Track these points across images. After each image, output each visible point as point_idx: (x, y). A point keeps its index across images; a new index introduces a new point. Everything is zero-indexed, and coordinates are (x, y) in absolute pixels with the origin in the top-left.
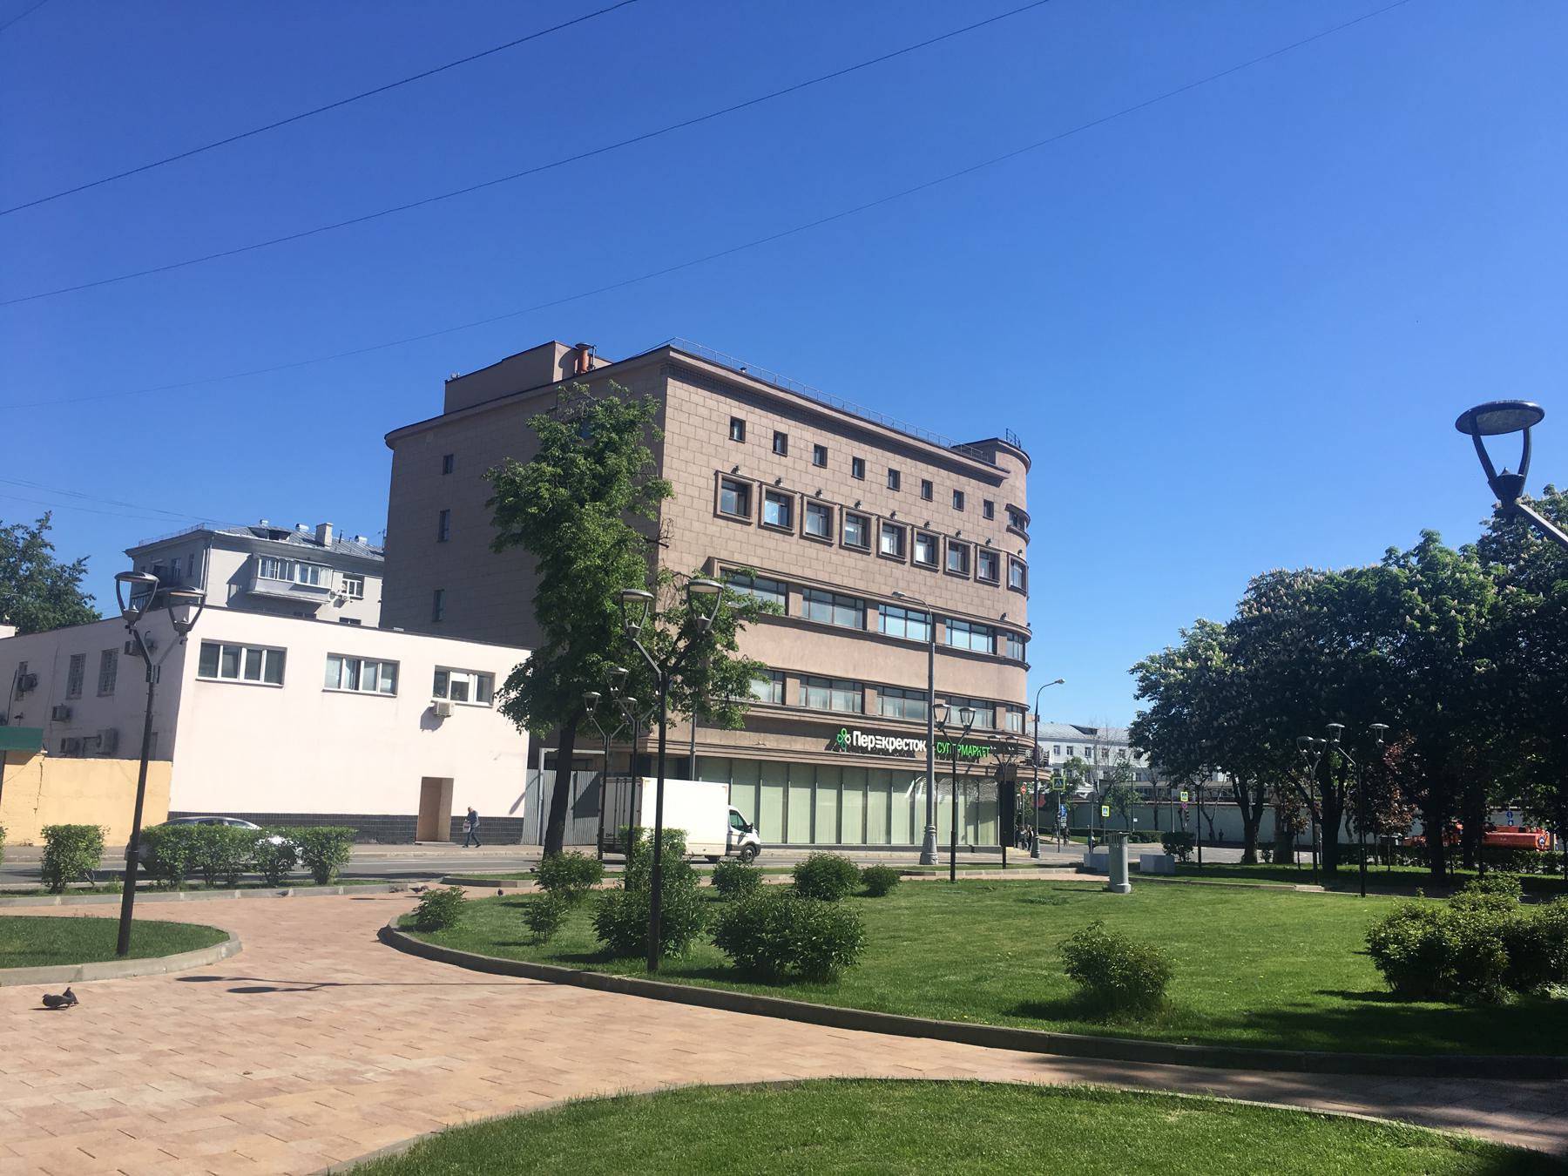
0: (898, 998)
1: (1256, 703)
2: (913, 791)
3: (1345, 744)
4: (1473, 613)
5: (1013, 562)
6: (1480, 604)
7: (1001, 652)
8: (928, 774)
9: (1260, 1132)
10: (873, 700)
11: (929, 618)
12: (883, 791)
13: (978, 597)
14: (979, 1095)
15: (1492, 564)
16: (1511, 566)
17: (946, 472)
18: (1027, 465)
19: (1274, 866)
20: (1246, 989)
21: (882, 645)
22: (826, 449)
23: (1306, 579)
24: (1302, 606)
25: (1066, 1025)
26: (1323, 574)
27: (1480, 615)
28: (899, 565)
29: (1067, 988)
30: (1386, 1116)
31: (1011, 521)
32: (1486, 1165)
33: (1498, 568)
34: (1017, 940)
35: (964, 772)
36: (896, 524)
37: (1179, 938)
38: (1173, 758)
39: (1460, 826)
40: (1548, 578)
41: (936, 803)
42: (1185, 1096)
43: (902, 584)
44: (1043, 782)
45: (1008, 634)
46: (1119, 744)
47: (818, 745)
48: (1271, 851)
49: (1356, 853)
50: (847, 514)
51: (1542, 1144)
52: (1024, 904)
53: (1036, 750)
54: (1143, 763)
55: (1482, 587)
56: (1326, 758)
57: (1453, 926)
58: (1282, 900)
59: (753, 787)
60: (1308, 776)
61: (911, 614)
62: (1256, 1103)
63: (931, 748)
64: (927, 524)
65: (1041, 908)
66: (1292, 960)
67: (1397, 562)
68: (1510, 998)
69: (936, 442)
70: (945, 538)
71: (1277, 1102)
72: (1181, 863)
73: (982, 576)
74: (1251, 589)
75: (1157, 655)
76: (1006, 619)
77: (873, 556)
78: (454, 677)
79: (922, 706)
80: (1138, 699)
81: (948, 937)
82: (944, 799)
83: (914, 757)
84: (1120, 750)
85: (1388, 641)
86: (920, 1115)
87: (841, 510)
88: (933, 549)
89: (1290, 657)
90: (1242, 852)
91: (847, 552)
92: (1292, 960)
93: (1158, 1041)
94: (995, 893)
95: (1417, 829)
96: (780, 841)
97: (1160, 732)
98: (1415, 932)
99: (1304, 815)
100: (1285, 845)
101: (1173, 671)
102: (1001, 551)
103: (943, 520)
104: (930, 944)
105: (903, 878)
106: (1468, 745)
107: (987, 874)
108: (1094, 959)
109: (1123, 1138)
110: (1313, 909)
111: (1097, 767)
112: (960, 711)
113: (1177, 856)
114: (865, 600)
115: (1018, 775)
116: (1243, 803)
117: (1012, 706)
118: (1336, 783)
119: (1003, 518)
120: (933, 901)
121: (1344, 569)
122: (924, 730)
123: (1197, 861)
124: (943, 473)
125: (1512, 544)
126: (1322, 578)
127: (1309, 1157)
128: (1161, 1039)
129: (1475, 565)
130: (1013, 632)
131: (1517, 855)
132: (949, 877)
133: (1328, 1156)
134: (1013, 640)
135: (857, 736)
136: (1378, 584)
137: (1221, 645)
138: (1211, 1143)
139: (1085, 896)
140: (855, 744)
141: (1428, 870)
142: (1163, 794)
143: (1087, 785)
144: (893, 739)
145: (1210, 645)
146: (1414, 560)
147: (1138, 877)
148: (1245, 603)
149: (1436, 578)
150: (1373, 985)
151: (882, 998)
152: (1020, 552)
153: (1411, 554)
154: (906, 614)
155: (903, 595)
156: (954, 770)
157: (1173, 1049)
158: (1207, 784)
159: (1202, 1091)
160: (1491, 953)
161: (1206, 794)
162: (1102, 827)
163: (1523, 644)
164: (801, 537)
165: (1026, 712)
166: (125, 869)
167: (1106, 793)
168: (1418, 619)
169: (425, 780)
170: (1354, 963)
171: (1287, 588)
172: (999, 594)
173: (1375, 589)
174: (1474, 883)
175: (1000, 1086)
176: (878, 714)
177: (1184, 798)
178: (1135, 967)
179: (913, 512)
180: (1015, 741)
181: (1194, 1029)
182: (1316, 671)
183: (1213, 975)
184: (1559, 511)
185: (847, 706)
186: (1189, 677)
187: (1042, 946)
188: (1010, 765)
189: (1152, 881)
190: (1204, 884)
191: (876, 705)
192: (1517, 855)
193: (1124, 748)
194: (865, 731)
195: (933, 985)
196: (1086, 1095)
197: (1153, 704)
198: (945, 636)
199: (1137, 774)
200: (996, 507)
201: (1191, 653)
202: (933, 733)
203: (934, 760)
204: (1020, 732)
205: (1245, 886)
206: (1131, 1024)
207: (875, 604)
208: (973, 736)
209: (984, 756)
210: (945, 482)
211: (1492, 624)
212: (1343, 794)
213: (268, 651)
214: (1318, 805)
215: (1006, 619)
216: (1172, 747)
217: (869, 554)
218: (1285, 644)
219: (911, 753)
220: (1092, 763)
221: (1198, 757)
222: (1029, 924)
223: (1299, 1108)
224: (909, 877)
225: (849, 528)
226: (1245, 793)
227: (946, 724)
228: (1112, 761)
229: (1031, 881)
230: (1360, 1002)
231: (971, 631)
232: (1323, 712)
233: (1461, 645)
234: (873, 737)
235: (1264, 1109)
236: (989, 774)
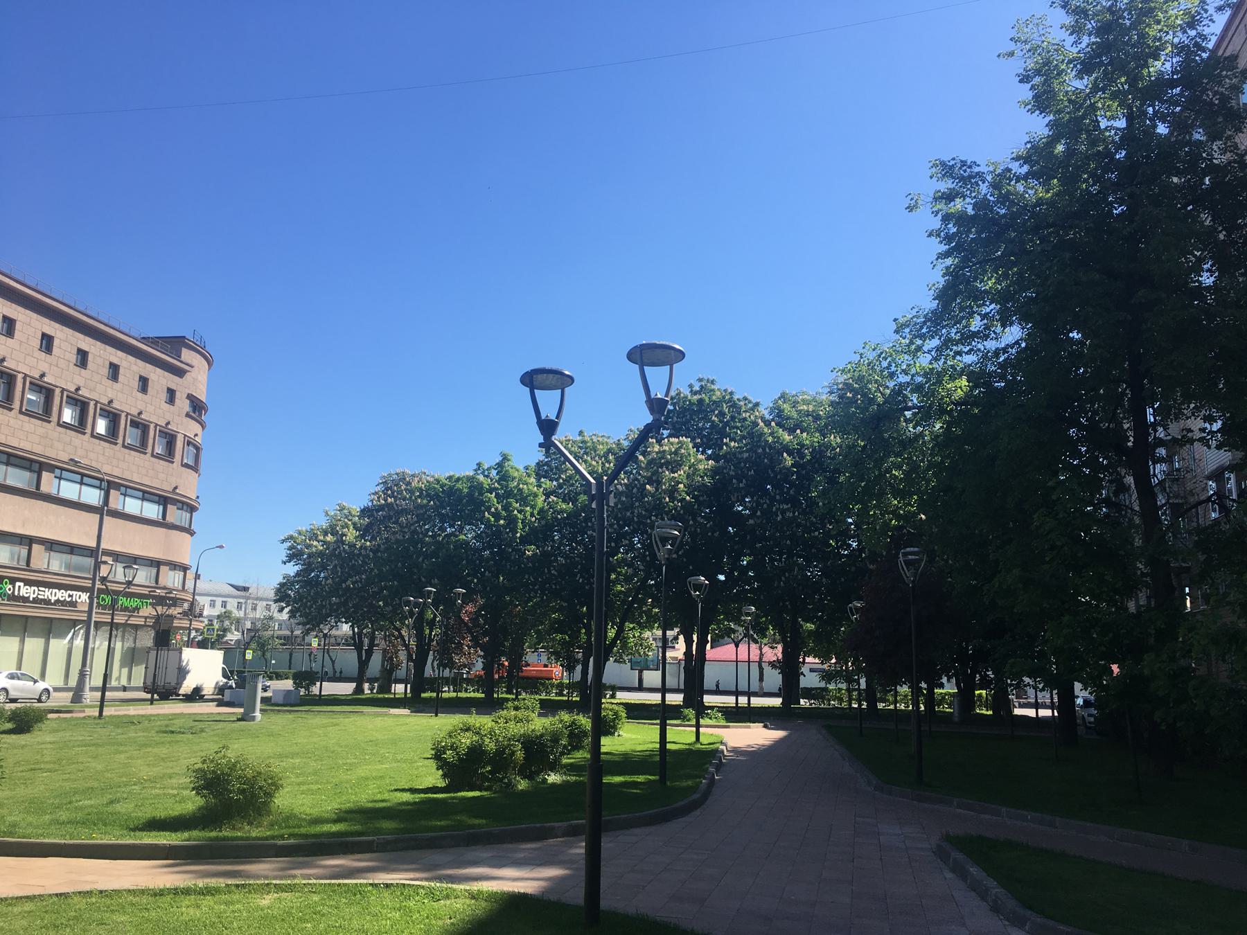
0: (30, 824)
1: (376, 570)
2: (72, 638)
3: (436, 604)
4: (528, 513)
5: (189, 443)
6: (533, 507)
7: (169, 519)
8: (87, 623)
9: (334, 903)
11: (104, 485)
12: (42, 638)
13: (153, 470)
14: (97, 902)
15: (543, 480)
16: (555, 483)
17: (134, 359)
18: (210, 363)
19: (376, 696)
20: (340, 792)
22: (15, 320)
23: (421, 479)
24: (416, 499)
25: (186, 835)
26: (433, 477)
27: (532, 515)
28: (80, 435)
29: (192, 803)
30: (427, 879)
31: (191, 409)
32: (490, 908)
33: (547, 484)
34: (154, 765)
35: (123, 622)
36: (80, 398)
37: (293, 755)
38: (308, 611)
39: (506, 663)
40: (576, 493)
41: (93, 649)
42: (278, 882)
43: (80, 452)
44: (197, 630)
45: (178, 504)
46: (267, 600)
48: (376, 684)
49: (435, 684)
50: (31, 383)
51: (527, 887)
52: (165, 735)
53: (192, 604)
54: (285, 616)
55: (536, 495)
56: (421, 614)
57: (492, 735)
58: (379, 722)
59: (43, 640)
60: (408, 626)
61: (86, 480)
62: (333, 881)
63: (93, 600)
64: (111, 402)
65: (179, 737)
66: (379, 767)
67: (483, 473)
68: (522, 785)
69: (126, 331)
70: (127, 416)
71: (351, 878)
72: (306, 695)
73: (159, 452)
74: (381, 483)
75: (304, 529)
76: (177, 491)
77: (53, 424)
79: (89, 562)
80: (285, 564)
81: (88, 767)
82: (100, 645)
83: (76, 607)
84: (267, 605)
85: (472, 529)
86: (36, 925)
87: (24, 379)
88: (115, 424)
89: (404, 536)
90: (354, 685)
92: (379, 767)
93: (253, 840)
94: (139, 727)
95: (479, 666)
96: (62, 684)
97: (301, 591)
98: (466, 740)
99: (403, 655)
100: (386, 679)
101: (315, 543)
102: (179, 433)
103: (127, 400)
104: (69, 773)
105: (50, 716)
106: (517, 606)
107: (135, 710)
108: (218, 777)
109: (221, 922)
110: (399, 727)
111: (246, 619)
112: (124, 568)
113: (303, 690)
114: (41, 463)
115: (174, 625)
116: (359, 648)
117: (175, 565)
118: (427, 632)
119: (183, 405)
120: (79, 735)
121: (447, 475)
122: (88, 584)
123: (318, 694)
124: (130, 358)
125: (556, 467)
126: (432, 480)
127: (368, 918)
128: (266, 838)
129: (533, 480)
130: (183, 503)
131: (541, 684)
132: (97, 714)
133: (382, 915)
134: (182, 509)
135: (19, 587)
136: (470, 488)
137: (354, 524)
138: (293, 917)
139: (221, 725)
140: (16, 593)
141: (483, 695)
142: (299, 640)
143: (236, 633)
144: (57, 590)
145: (346, 524)
146: (494, 473)
147: (268, 708)
148: (376, 493)
149: (507, 487)
150: (434, 782)
151: (14, 825)
152: (196, 435)
153: (493, 468)
154: (82, 479)
155: (80, 462)
156: (112, 619)
157: (275, 845)
158: (334, 632)
159: (293, 876)
160: (513, 753)
161: (332, 640)
162: (245, 668)
163: (557, 537)
164: (124, 446)
165: (188, 571)
166: (660, 702)
167: (251, 640)
168: (493, 515)
170: (422, 766)
171: (407, 485)
172: (173, 469)
173: (467, 491)
174: (510, 704)
175: (117, 892)
176: (44, 567)
177: (315, 643)
178: (252, 782)
179: (96, 387)
180: (173, 596)
181: (294, 827)
182: (422, 549)
183: (317, 783)
184: (586, 448)
185: (12, 558)
186: (328, 548)
187: (176, 770)
188: (168, 616)
189: (279, 711)
190: (320, 711)
191: (40, 558)
192: (541, 684)
193: (271, 603)
194: (28, 583)
195: (68, 809)
196: (195, 891)
197: (297, 568)
198: (116, 500)
199: (279, 625)
200: (178, 395)
201: (332, 530)
202: (97, 586)
203: (94, 610)
204: (180, 588)
205: (353, 712)
206: (244, 828)
207: (51, 468)
208: (133, 590)
209: (145, 607)
210: (132, 367)
211: (539, 522)
212: (431, 640)
214: (413, 648)
215: (177, 491)
216: (309, 603)
217: (50, 422)
218: (402, 527)
219: (73, 604)
220: (242, 615)
221: (328, 611)
222: (166, 751)
223: (365, 881)
224: (58, 714)
225: (31, 396)
226: (361, 642)
227: (110, 578)
228: (260, 613)
229: (175, 714)
230: (422, 795)
231: (143, 499)
232: (423, 579)
233: (518, 535)
234: (36, 588)
235: (339, 885)
236: (148, 624)
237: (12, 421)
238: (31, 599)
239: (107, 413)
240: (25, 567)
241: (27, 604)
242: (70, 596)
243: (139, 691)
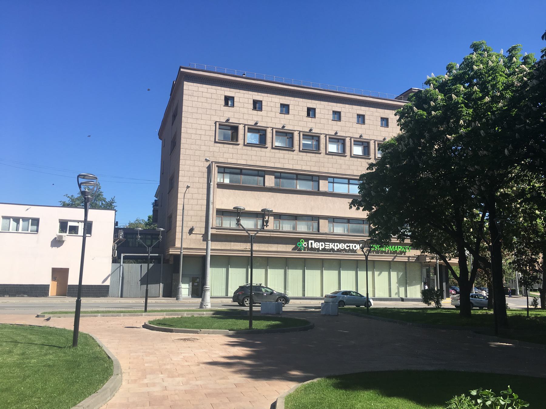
10: (325, 226)
21: (228, 190)
47: (289, 248)
61: (351, 181)
78: (70, 224)
91: (305, 154)
115: (170, 253)
135: (312, 243)
140: (310, 246)
144: (338, 244)
154: (349, 181)
156: (252, 254)
166: (249, 310)
169: (68, 269)
194: (316, 240)
207: (325, 178)
213: (32, 220)
219: (354, 251)
236: (410, 261)
237: (295, 157)
238: (321, 249)
239: (337, 140)
240: (317, 232)
241: (334, 253)
242: (347, 246)
243: (419, 301)
